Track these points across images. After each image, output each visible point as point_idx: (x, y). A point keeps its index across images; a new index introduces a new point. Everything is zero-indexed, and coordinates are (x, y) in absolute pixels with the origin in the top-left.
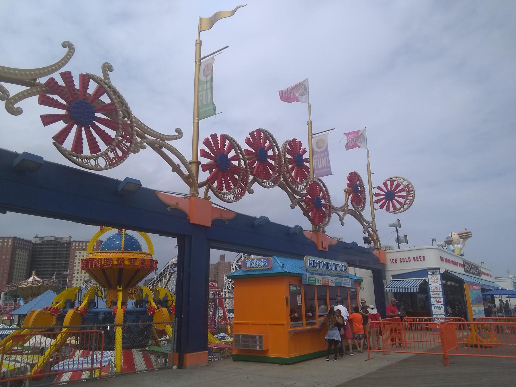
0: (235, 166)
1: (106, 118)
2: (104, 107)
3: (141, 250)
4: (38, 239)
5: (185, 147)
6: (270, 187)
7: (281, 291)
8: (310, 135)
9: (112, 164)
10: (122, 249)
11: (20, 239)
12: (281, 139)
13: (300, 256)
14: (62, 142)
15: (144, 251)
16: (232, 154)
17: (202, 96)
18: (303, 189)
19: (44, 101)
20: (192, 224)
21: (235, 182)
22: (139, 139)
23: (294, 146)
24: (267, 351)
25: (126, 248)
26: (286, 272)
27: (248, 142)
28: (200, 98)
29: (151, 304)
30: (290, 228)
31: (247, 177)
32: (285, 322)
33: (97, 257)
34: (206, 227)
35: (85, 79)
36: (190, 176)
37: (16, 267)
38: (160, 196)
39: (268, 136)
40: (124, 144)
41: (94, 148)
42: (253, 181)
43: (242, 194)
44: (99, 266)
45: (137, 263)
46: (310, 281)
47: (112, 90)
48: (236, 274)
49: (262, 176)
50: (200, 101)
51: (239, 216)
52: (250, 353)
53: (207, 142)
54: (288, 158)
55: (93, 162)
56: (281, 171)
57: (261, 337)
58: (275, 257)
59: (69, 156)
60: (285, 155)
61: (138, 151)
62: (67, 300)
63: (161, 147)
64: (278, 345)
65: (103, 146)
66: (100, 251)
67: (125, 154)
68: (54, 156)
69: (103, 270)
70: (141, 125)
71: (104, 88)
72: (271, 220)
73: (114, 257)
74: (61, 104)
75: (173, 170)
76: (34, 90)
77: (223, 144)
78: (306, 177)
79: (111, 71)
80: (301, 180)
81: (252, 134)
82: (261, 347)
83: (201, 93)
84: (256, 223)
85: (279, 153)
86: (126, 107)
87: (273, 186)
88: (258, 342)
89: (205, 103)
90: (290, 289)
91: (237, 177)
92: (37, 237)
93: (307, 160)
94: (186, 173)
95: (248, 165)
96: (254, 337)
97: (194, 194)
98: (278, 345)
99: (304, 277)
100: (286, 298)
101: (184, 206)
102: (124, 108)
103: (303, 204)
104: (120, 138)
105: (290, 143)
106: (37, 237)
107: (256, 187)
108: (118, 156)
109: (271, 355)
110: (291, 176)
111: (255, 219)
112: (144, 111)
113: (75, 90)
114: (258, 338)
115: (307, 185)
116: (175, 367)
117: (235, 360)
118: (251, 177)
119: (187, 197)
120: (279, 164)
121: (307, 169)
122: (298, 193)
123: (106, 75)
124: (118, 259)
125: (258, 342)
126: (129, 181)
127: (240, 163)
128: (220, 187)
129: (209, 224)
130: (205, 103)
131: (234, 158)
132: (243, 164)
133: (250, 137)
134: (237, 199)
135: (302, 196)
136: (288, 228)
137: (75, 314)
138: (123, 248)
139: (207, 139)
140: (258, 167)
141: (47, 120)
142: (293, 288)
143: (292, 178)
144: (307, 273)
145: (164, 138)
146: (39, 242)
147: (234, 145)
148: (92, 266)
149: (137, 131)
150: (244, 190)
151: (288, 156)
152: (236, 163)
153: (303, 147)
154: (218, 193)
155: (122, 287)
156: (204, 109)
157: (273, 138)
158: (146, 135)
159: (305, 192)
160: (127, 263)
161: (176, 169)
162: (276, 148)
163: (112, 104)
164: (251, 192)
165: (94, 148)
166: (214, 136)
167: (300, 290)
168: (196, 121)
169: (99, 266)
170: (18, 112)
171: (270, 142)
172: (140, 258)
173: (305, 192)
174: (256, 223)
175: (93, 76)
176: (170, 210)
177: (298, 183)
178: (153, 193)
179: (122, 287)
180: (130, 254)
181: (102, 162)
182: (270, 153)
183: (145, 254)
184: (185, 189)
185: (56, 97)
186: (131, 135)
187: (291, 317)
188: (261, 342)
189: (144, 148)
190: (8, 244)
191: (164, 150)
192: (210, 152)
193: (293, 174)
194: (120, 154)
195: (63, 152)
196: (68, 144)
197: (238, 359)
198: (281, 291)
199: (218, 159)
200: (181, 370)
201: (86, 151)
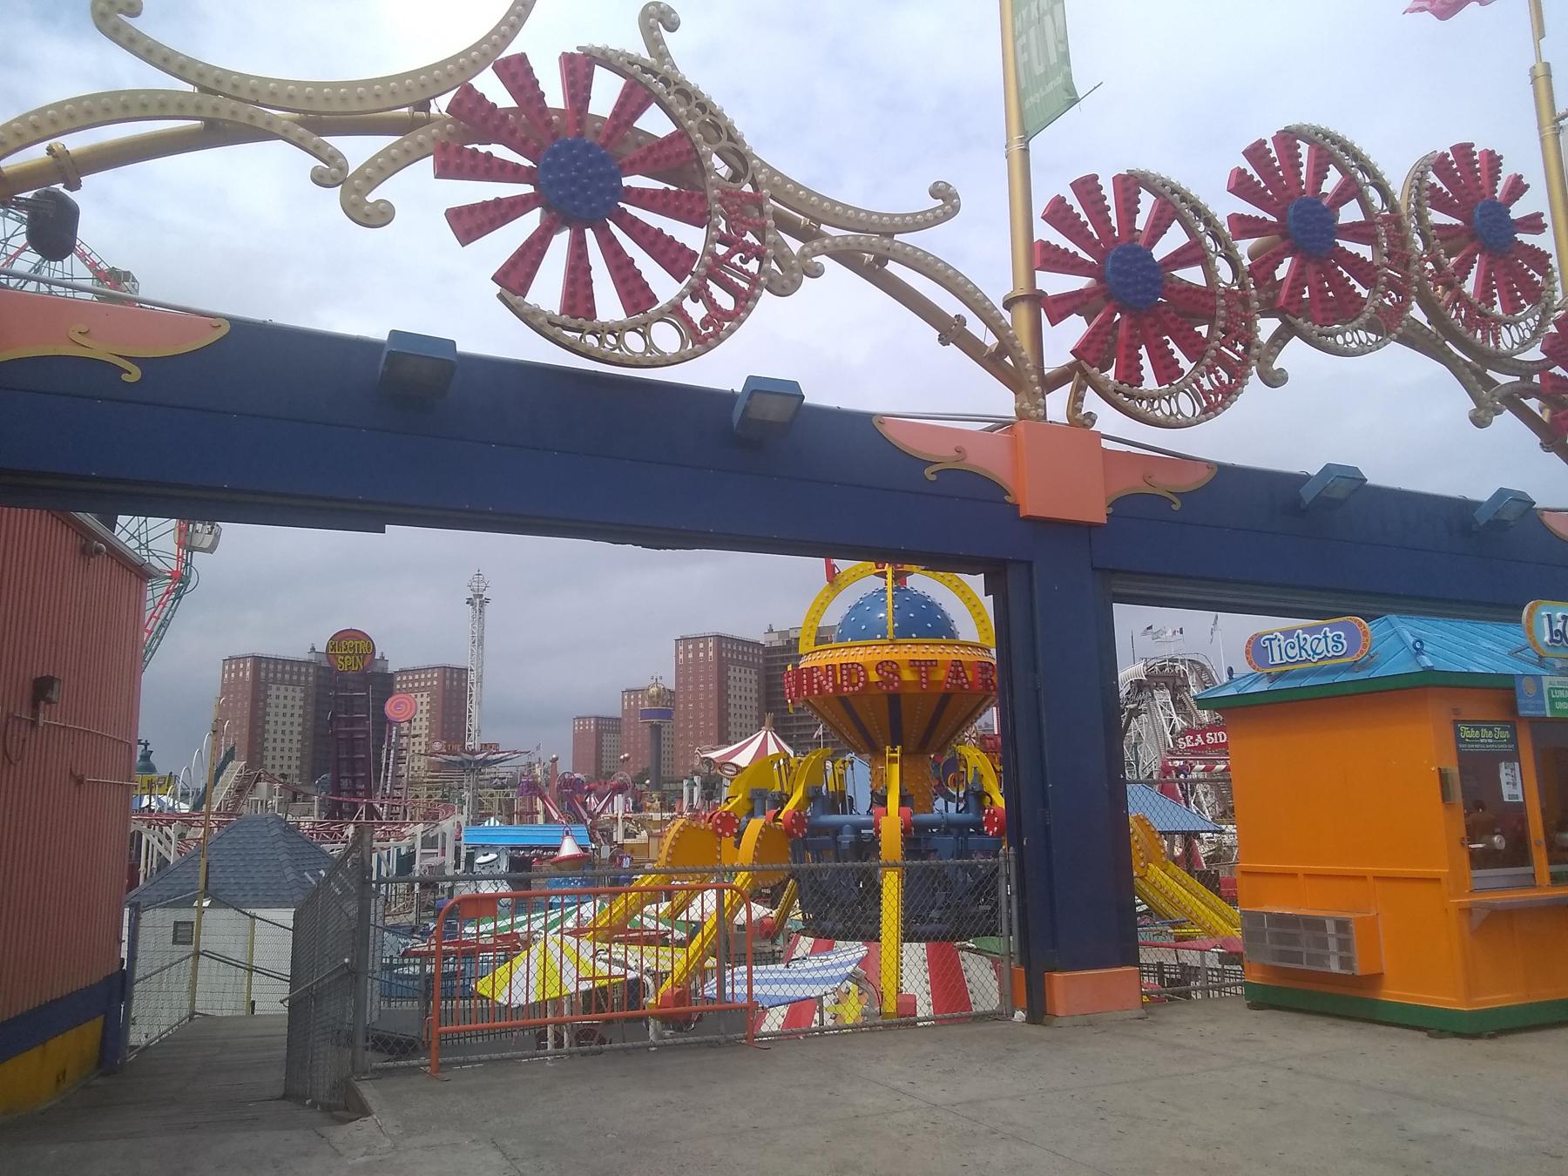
0: (1190, 288)
1: (660, 185)
2: (651, 150)
3: (952, 634)
4: (774, 637)
5: (984, 250)
6: (1363, 350)
7: (1421, 749)
8: (1547, 119)
9: (701, 339)
10: (890, 635)
11: (733, 640)
12: (1397, 150)
13: (1503, 607)
14: (523, 289)
15: (962, 638)
16: (1174, 238)
17: (1025, 48)
18: (1525, 345)
19: (453, 165)
20: (1031, 520)
21: (1195, 349)
22: (795, 245)
23: (1465, 178)
24: (1375, 980)
25: (903, 631)
26: (1429, 671)
27: (1240, 185)
28: (1023, 58)
29: (992, 802)
30: (1478, 504)
31: (1250, 323)
32: (1442, 871)
33: (823, 664)
34: (1091, 526)
35: (578, 69)
36: (1002, 350)
37: (732, 710)
38: (889, 432)
39: (1329, 149)
40: (734, 266)
41: (635, 293)
42: (1280, 339)
43: (1228, 393)
44: (829, 688)
45: (941, 675)
46: (1559, 706)
47: (673, 89)
48: (1231, 691)
49: (1324, 311)
50: (1022, 73)
51: (1226, 475)
52: (1309, 984)
53: (1057, 214)
54: (1439, 227)
55: (634, 342)
56: (1407, 279)
57: (1342, 926)
58: (1393, 618)
59: (550, 330)
60: (1421, 218)
61: (796, 285)
62: (753, 791)
63: (882, 260)
64: (1422, 956)
65: (664, 286)
66: (834, 645)
67: (745, 301)
68: (489, 332)
69: (844, 701)
70: (785, 189)
71: (646, 87)
72: (1373, 479)
73: (870, 658)
74: (517, 167)
75: (944, 341)
76: (420, 137)
77: (1128, 208)
78: (1535, 294)
79: (672, 27)
80: (1512, 306)
81: (1256, 153)
82: (1345, 962)
83: (1023, 39)
84: (1308, 494)
85: (1394, 208)
86: (730, 138)
87: (1377, 346)
88: (1333, 944)
89: (1039, 70)
90: (1459, 740)
91: (1203, 330)
92: (771, 631)
93: (1533, 224)
94: (991, 341)
95: (1250, 274)
96: (1317, 924)
97: (1030, 414)
98: (1422, 956)
99: (1527, 688)
100: (1443, 776)
101: (992, 462)
102: (724, 143)
103: (1533, 404)
104: (721, 250)
105: (1440, 164)
106: (771, 631)
107: (1296, 355)
108: (718, 309)
109: (1391, 993)
110: (1460, 297)
111: (1301, 480)
112: (794, 135)
113: (544, 110)
114: (1331, 927)
115: (1542, 324)
116: (1020, 1015)
117: (1254, 1006)
118: (1267, 327)
119: (1003, 424)
120: (1399, 254)
121: (1539, 259)
122: (1504, 362)
123: (654, 43)
124: (880, 666)
125: (1333, 944)
126: (758, 387)
127: (1210, 273)
128: (1131, 375)
129: (1099, 515)
130: (1039, 70)
131: (1181, 258)
132: (1225, 272)
133: (1245, 164)
134: (1211, 410)
135: (1526, 370)
136: (1463, 507)
137: (766, 832)
138: (891, 631)
139: (1059, 201)
140: (1297, 279)
141: (470, 224)
142: (1473, 734)
143: (1469, 305)
144: (1542, 672)
145: (888, 227)
146: (779, 644)
147: (1175, 205)
148: (810, 690)
149: (777, 216)
150: (1238, 374)
151: (1437, 217)
152: (1193, 275)
153: (1506, 173)
154: (1125, 398)
155: (898, 748)
156: (1040, 90)
157: (1356, 156)
158: (823, 227)
159: (1535, 354)
160: (907, 675)
161: (951, 332)
162: (1373, 193)
163: (681, 135)
164: (1274, 379)
165: (635, 293)
166: (1087, 188)
167: (1513, 740)
168: (1016, 147)
169: (829, 688)
170: (379, 217)
171: (1342, 169)
172: (946, 657)
173: (1535, 354)
174: (1308, 494)
175: (604, 52)
176: (934, 478)
177: (1499, 321)
178: (863, 423)
179: (898, 748)
180: (914, 649)
181: (666, 337)
182: (1350, 213)
183: (964, 645)
184: (1000, 401)
185: (500, 152)
186: (760, 227)
187: (1472, 853)
188: (1344, 945)
189: (816, 272)
190: (706, 654)
191: (893, 267)
192: (1072, 248)
193: (1469, 286)
194: (726, 301)
195: (531, 318)
196: (547, 290)
197: (1263, 999)
198: (1421, 749)
199: (1109, 266)
200: (1034, 1030)
201: (608, 304)
